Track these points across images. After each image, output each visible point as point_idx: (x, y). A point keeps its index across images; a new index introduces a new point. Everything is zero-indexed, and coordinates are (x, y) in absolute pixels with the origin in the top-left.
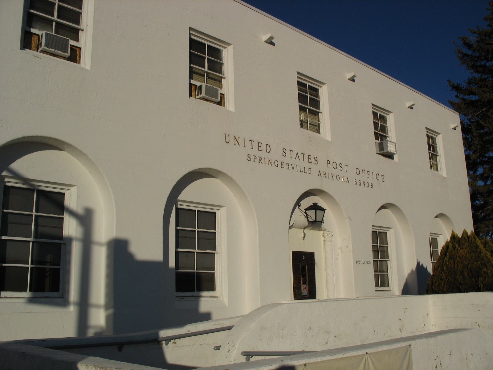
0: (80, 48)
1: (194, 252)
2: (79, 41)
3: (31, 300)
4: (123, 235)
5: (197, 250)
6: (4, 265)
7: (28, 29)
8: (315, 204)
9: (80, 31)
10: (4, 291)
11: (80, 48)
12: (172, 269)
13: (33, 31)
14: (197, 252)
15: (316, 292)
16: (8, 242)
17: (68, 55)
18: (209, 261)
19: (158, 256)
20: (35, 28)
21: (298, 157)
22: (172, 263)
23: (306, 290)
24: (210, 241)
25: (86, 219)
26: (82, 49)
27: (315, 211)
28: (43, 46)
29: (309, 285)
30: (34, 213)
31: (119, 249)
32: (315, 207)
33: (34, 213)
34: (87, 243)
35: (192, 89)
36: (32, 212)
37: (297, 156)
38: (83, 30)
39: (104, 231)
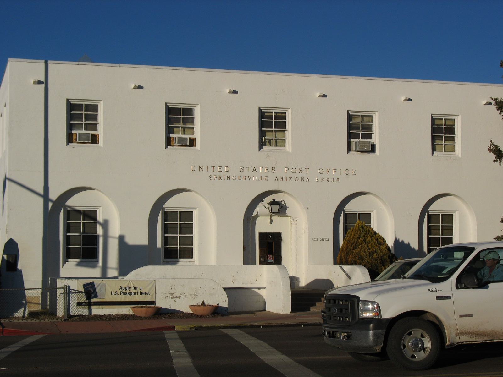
0: (99, 134)
1: (443, 136)
2: (98, 130)
3: (78, 264)
4: (123, 233)
5: (444, 135)
6: (69, 246)
7: (70, 132)
8: (274, 200)
9: (98, 124)
10: (70, 258)
11: (99, 134)
12: (159, 249)
13: (73, 132)
14: (444, 136)
15: (281, 260)
16: (71, 236)
17: (91, 142)
18: (190, 241)
19: (144, 241)
20: (74, 130)
21: (256, 170)
22: (159, 244)
23: (272, 258)
24: (190, 229)
25: (105, 225)
26: (99, 134)
27: (41, 288)
28: (78, 141)
29: (274, 255)
30: (82, 222)
31: (121, 239)
32: (274, 203)
33: (82, 222)
34: (106, 236)
35: (171, 140)
36: (81, 221)
37: (254, 169)
38: (99, 124)
39: (115, 231)
